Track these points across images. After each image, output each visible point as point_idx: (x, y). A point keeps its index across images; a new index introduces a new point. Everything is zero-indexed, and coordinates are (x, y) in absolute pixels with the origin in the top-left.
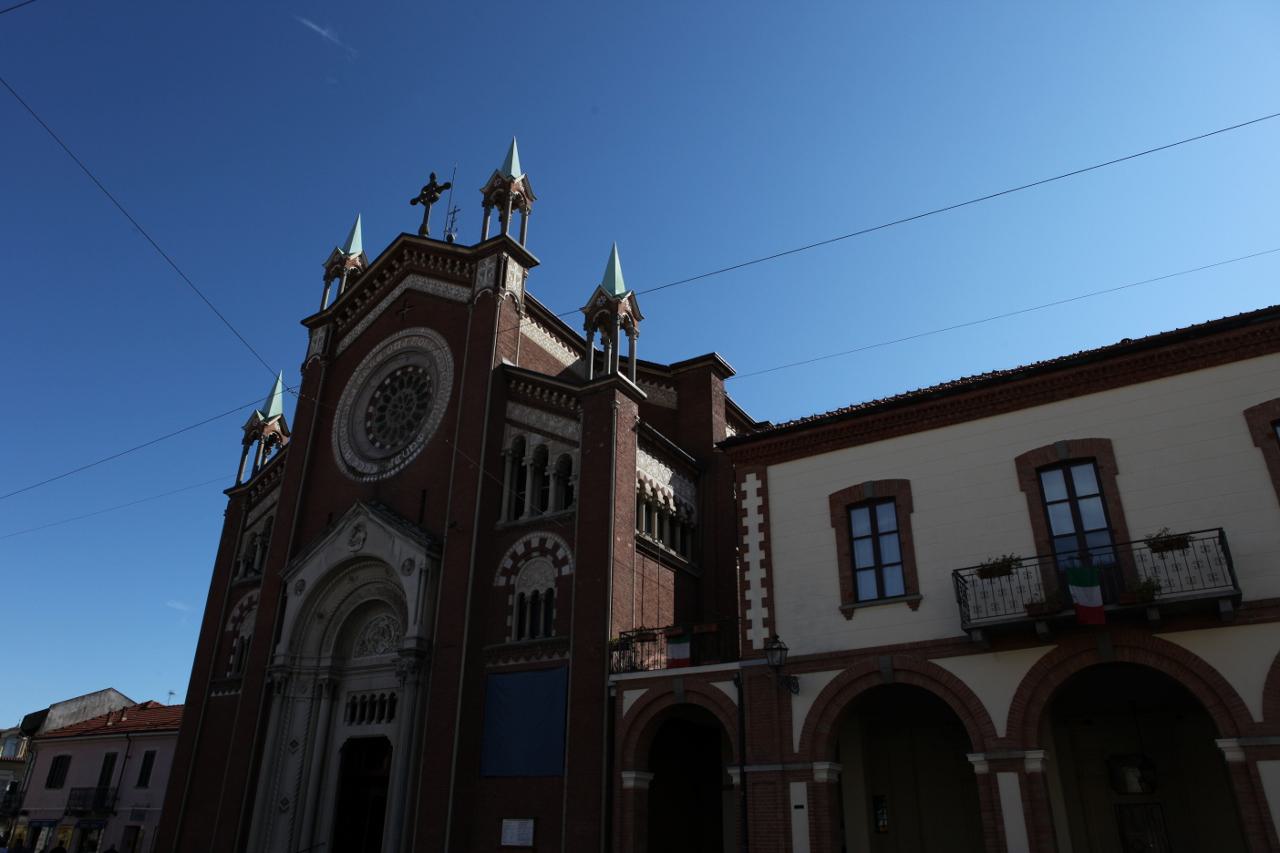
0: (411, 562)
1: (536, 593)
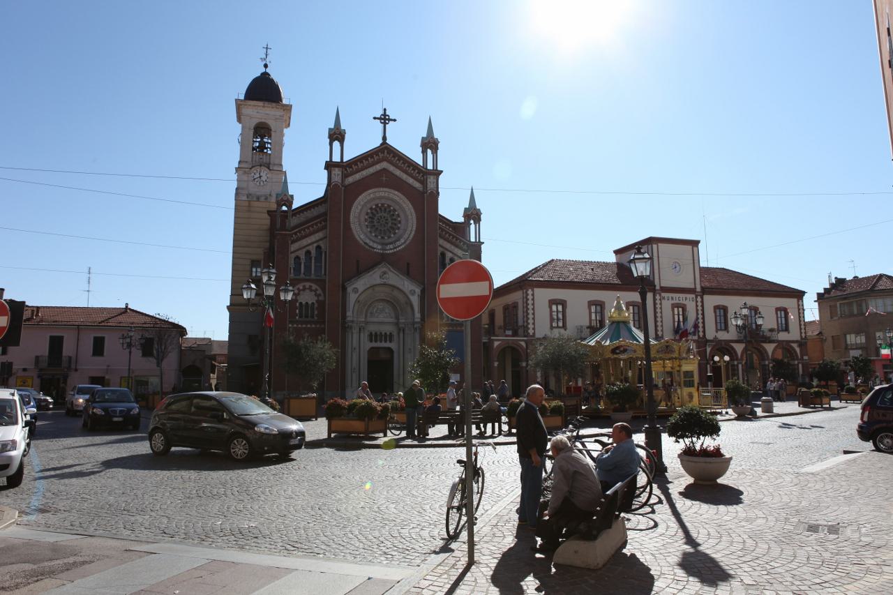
0: (414, 291)
1: (307, 303)
